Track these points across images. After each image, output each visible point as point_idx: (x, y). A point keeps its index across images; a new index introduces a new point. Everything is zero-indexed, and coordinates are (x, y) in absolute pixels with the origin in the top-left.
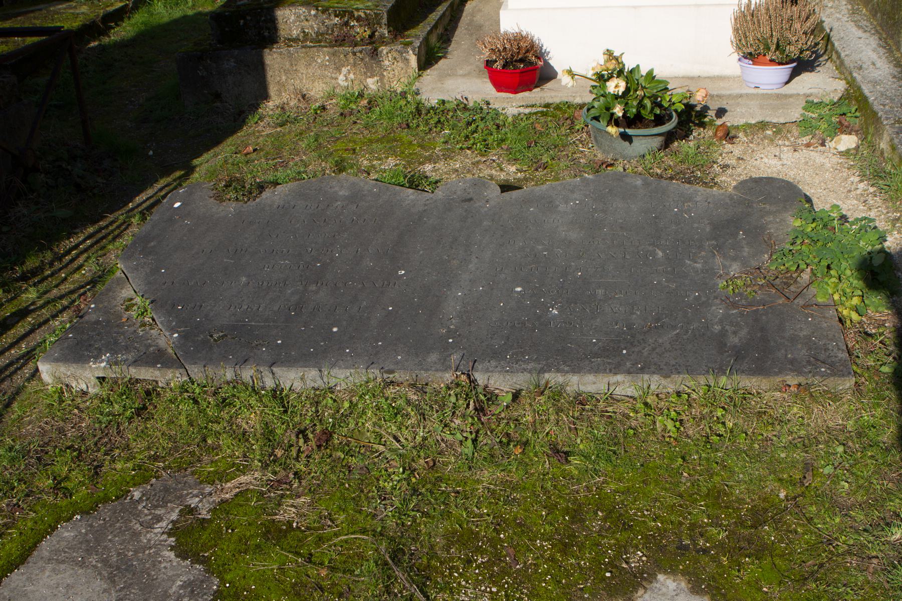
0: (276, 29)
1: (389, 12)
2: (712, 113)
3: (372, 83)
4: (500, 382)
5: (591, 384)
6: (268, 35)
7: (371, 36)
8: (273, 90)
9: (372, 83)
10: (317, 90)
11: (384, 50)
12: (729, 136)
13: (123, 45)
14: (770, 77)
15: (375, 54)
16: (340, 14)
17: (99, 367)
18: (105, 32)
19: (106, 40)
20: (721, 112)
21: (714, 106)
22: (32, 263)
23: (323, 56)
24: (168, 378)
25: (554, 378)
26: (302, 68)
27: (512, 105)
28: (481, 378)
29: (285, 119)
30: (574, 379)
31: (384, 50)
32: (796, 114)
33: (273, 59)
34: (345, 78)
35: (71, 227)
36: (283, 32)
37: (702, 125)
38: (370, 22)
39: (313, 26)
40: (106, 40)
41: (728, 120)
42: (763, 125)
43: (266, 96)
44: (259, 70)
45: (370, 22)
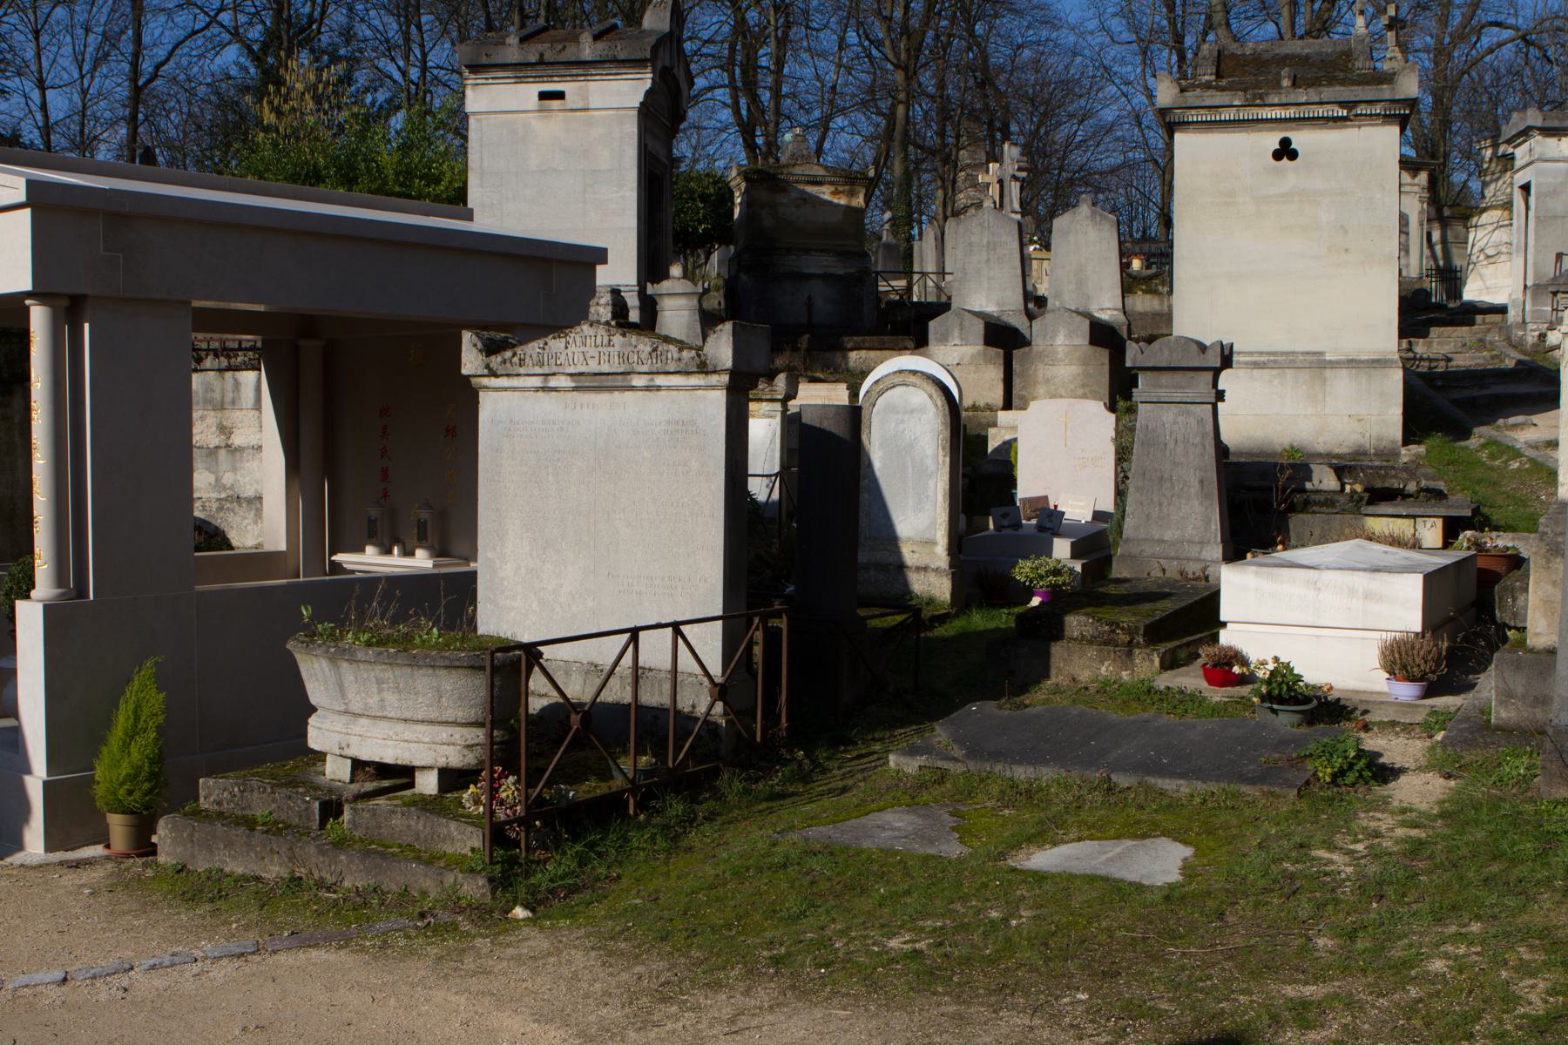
0: (1062, 630)
1: (1146, 627)
2: (1358, 712)
3: (1125, 675)
4: (1122, 780)
5: (1168, 784)
6: (1057, 633)
7: (1130, 642)
8: (1053, 672)
9: (1125, 675)
10: (1084, 676)
11: (1137, 651)
12: (1366, 728)
13: (944, 640)
14: (1406, 691)
15: (1130, 654)
16: (1110, 624)
17: (921, 760)
18: (931, 628)
19: (929, 634)
20: (1366, 712)
21: (1361, 708)
22: (877, 735)
23: (1092, 652)
24: (958, 768)
25: (1152, 780)
26: (1076, 659)
27: (1217, 695)
28: (1114, 777)
29: (1057, 690)
30: (1160, 781)
31: (1137, 651)
32: (1419, 718)
33: (1057, 649)
34: (1105, 670)
35: (905, 723)
36: (1067, 633)
37: (1349, 720)
38: (1131, 631)
39: (1089, 631)
40: (929, 634)
41: (1368, 718)
42: (1393, 724)
43: (1047, 676)
44: (1046, 657)
45: (1131, 631)
